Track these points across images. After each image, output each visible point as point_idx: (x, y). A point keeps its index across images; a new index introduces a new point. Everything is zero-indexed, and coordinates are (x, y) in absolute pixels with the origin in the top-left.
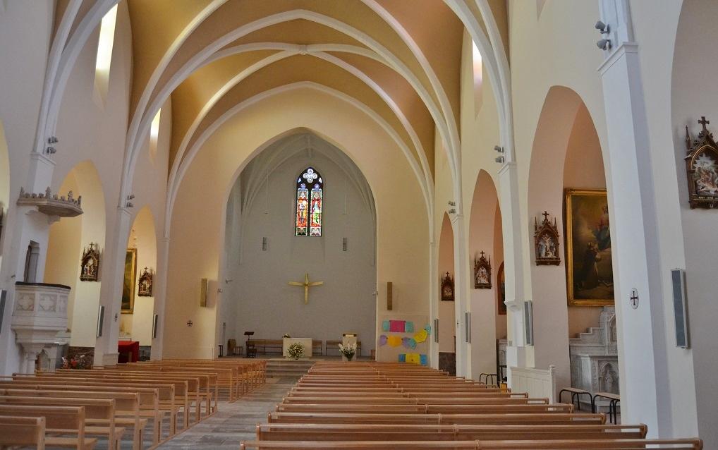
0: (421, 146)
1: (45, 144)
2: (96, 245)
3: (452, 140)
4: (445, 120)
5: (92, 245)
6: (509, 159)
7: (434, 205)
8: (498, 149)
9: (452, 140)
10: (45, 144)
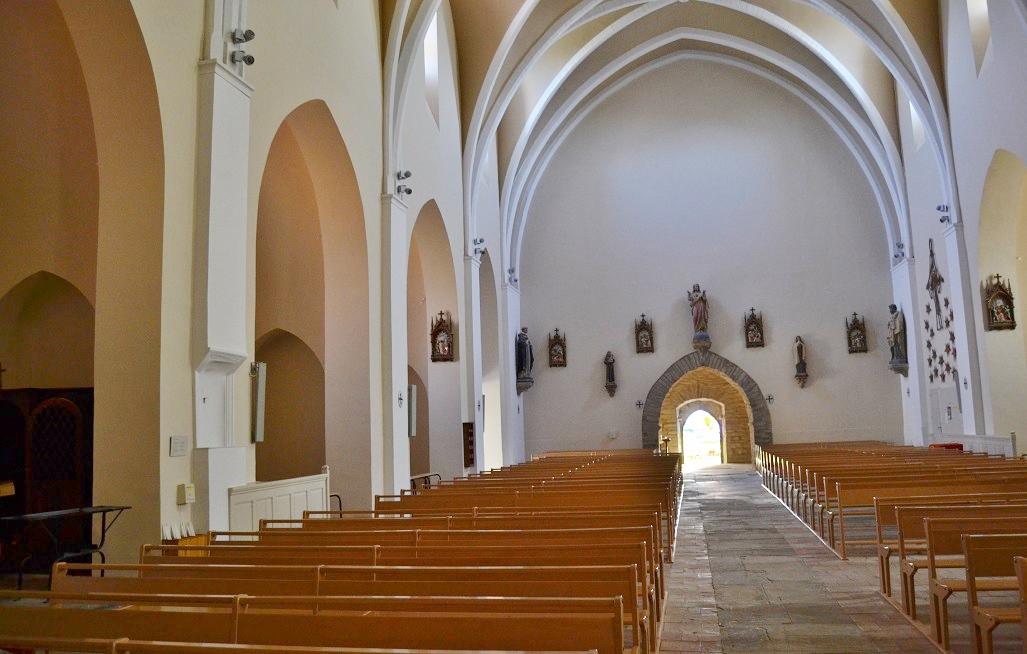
0: (799, 66)
1: (226, 45)
2: (448, 313)
3: (942, 141)
4: (926, 97)
5: (441, 314)
6: (954, 220)
7: (906, 196)
8: (481, 241)
9: (939, 128)
10: (226, 45)
